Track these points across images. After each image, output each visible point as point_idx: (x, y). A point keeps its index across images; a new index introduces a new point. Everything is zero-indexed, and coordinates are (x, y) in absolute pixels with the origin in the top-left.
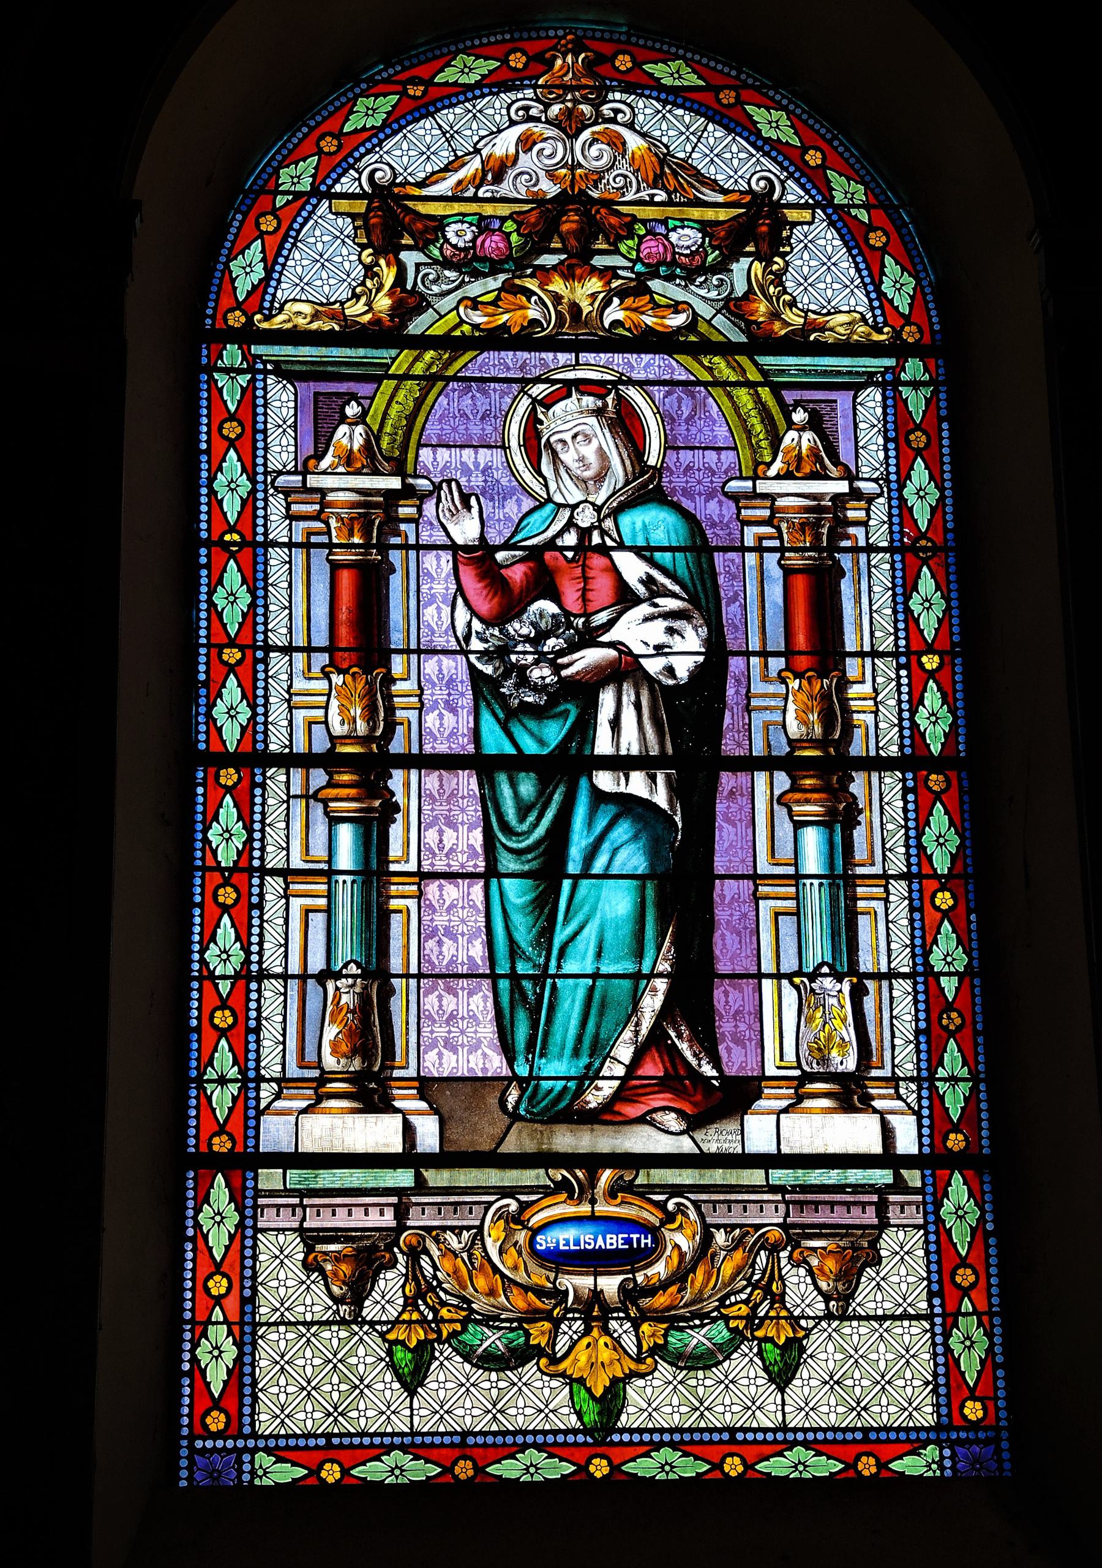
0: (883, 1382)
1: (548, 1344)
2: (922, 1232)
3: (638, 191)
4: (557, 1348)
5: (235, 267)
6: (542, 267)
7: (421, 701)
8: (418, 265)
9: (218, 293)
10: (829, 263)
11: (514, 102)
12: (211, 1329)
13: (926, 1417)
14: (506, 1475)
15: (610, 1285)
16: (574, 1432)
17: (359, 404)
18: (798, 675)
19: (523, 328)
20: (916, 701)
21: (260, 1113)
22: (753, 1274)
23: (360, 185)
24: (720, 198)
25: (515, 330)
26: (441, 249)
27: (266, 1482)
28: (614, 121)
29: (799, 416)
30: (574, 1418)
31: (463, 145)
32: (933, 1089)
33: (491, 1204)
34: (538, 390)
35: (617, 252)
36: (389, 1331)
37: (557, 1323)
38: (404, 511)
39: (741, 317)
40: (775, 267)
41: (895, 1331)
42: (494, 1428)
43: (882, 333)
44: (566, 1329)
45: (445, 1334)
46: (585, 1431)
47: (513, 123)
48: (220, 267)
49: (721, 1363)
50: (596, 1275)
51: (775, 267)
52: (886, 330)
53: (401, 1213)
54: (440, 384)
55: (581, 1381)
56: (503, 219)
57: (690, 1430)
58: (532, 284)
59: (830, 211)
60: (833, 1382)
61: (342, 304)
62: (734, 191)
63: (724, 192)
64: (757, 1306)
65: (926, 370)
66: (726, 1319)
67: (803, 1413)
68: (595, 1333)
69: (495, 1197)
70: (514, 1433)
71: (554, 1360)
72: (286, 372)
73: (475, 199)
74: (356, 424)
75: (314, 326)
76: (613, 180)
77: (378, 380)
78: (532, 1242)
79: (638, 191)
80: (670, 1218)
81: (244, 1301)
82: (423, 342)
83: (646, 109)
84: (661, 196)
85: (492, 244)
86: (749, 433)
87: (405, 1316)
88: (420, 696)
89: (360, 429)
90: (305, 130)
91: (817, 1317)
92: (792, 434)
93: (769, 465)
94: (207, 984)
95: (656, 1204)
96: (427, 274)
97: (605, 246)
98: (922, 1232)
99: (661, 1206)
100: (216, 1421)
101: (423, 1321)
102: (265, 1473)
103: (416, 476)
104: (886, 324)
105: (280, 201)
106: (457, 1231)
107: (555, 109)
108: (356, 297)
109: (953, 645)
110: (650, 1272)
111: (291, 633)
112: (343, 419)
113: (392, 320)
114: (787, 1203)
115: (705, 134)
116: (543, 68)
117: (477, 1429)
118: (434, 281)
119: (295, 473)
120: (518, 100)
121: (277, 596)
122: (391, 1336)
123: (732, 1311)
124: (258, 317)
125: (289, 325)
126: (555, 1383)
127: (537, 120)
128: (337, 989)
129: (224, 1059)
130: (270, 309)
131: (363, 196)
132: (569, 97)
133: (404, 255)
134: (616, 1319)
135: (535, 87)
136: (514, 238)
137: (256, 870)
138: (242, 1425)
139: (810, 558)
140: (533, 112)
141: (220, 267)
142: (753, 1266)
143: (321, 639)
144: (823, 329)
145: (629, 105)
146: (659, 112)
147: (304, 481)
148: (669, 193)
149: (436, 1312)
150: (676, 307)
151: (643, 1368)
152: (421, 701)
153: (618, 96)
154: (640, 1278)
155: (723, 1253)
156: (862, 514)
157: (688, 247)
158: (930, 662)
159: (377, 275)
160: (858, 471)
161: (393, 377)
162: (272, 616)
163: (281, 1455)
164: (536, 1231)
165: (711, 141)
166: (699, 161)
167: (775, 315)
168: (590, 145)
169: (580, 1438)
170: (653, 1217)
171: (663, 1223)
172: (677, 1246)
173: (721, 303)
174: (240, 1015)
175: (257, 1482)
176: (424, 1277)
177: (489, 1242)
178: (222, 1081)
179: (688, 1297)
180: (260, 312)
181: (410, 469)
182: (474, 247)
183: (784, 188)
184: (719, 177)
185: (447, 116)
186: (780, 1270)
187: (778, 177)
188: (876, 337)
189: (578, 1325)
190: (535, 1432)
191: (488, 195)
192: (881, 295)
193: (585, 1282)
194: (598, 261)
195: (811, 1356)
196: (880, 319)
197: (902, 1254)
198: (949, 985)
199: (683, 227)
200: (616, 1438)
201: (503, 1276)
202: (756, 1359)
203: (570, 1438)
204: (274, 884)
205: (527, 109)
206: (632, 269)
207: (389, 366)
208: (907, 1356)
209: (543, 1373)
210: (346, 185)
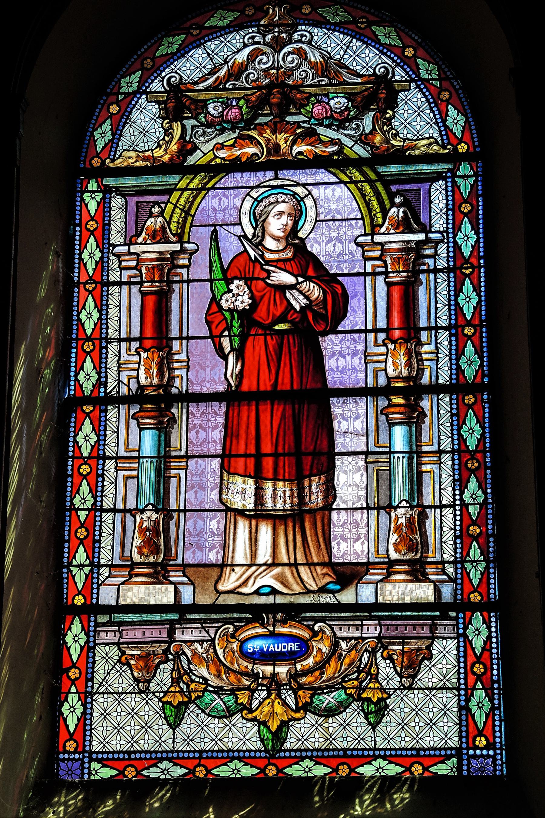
0: (431, 724)
1: (247, 702)
2: (456, 641)
3: (313, 79)
4: (253, 706)
5: (97, 135)
6: (260, 124)
7: (188, 365)
8: (193, 127)
9: (87, 148)
10: (419, 112)
11: (246, 35)
12: (70, 696)
13: (454, 742)
14: (223, 775)
15: (282, 670)
16: (260, 751)
17: (160, 206)
18: (394, 342)
19: (248, 158)
20: (460, 353)
21: (99, 585)
22: (360, 664)
23: (163, 84)
24: (359, 80)
25: (244, 159)
26: (205, 117)
27: (97, 777)
28: (300, 41)
29: (397, 200)
30: (259, 743)
31: (218, 60)
32: (463, 568)
33: (219, 628)
34: (255, 193)
35: (300, 113)
36: (163, 697)
37: (253, 692)
38: (183, 261)
39: (367, 144)
40: (388, 115)
41: (438, 695)
42: (216, 748)
43: (446, 149)
44: (257, 696)
45: (193, 697)
46: (266, 751)
47: (245, 46)
48: (89, 134)
49: (341, 713)
50: (275, 665)
51: (388, 115)
52: (449, 147)
53: (171, 633)
54: (204, 192)
55: (265, 723)
56: (239, 99)
57: (325, 750)
58: (254, 134)
59: (419, 83)
60: (403, 725)
61: (152, 150)
62: (366, 75)
63: (359, 76)
64: (362, 682)
65: (472, 169)
66: (345, 689)
67: (387, 741)
68: (273, 697)
69: (220, 624)
70: (228, 751)
71: (251, 711)
72: (121, 192)
73: (225, 89)
74: (158, 216)
75: (137, 164)
76: (299, 74)
77: (169, 192)
78: (241, 648)
79: (313, 79)
80: (315, 634)
81: (88, 680)
82: (195, 170)
83: (318, 33)
84: (325, 81)
85: (234, 113)
86: (370, 210)
87: (172, 689)
88: (188, 362)
89: (160, 219)
90: (135, 57)
91: (394, 688)
92: (394, 210)
93: (381, 226)
94: (73, 512)
95: (308, 626)
96: (197, 132)
97: (293, 110)
98: (456, 641)
99: (311, 628)
100: (71, 746)
101: (182, 692)
102: (96, 773)
103: (188, 242)
104: (449, 144)
105: (121, 97)
106: (201, 642)
107: (269, 38)
108: (159, 146)
109: (481, 321)
110: (304, 663)
111: (120, 295)
112: (151, 215)
113: (178, 158)
114: (381, 626)
115: (351, 45)
116: (263, 14)
117: (207, 749)
118: (201, 136)
119: (125, 245)
120: (249, 33)
121: (113, 312)
122: (164, 700)
123: (349, 685)
124: (108, 161)
125: (125, 164)
126: (249, 725)
127: (259, 43)
128: (142, 518)
129: (81, 556)
130: (114, 156)
131: (166, 91)
132: (276, 30)
133: (185, 122)
134: (284, 689)
135: (258, 26)
136: (244, 109)
137: (103, 339)
138: (85, 746)
139: (402, 277)
140: (257, 39)
141: (89, 134)
142: (360, 660)
143: (136, 333)
144: (413, 148)
145: (309, 32)
146: (326, 34)
147: (129, 249)
148: (329, 79)
149: (188, 686)
150: (333, 142)
151: (297, 715)
152: (188, 365)
153: (303, 27)
154: (299, 667)
155: (344, 653)
156: (432, 251)
157: (340, 108)
158: (468, 331)
159: (171, 133)
160: (431, 226)
161: (179, 190)
162: (110, 311)
163: (104, 763)
164: (243, 642)
165: (354, 48)
166: (347, 60)
167: (387, 141)
168: (288, 56)
169: (263, 755)
170: (306, 635)
171: (311, 638)
172: (319, 650)
173: (357, 138)
174: (91, 532)
175: (92, 777)
176: (182, 667)
177: (218, 648)
178: (81, 566)
179: (325, 677)
180: (109, 158)
181: (185, 239)
182: (222, 116)
183: (394, 72)
184: (358, 67)
185: (211, 45)
186: (376, 659)
187: (391, 66)
188: (442, 151)
189: (264, 694)
190: (238, 751)
191: (231, 87)
192: (446, 127)
193: (268, 669)
194: (289, 118)
195: (391, 710)
196: (446, 141)
197: (444, 653)
198: (473, 510)
199: (337, 97)
200: (282, 754)
201: (224, 665)
202: (361, 712)
203: (258, 754)
204: (110, 465)
205: (253, 38)
206: (309, 122)
207: (177, 185)
208: (445, 710)
209: (243, 718)
210: (156, 86)
